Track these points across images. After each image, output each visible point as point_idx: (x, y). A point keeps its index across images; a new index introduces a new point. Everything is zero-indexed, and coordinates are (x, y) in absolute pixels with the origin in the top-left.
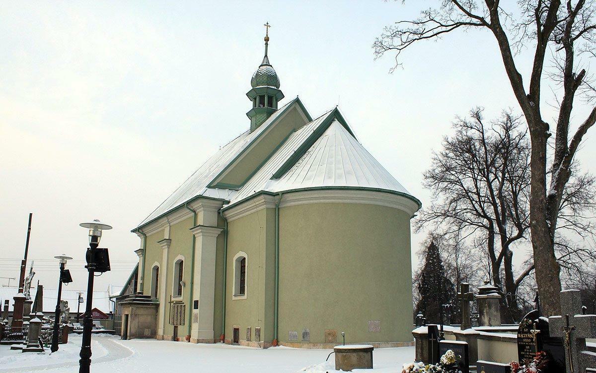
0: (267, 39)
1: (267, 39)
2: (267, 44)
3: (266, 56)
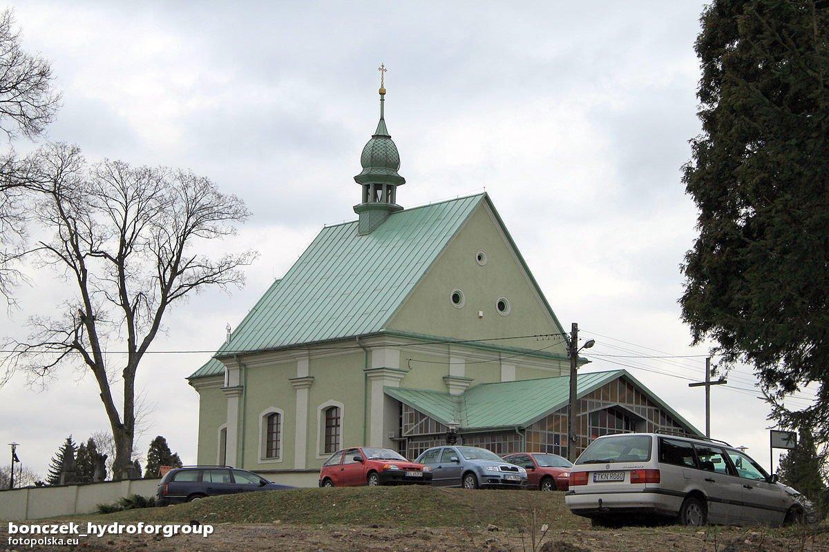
0: (382, 93)
1: (382, 93)
2: (382, 100)
3: (382, 119)
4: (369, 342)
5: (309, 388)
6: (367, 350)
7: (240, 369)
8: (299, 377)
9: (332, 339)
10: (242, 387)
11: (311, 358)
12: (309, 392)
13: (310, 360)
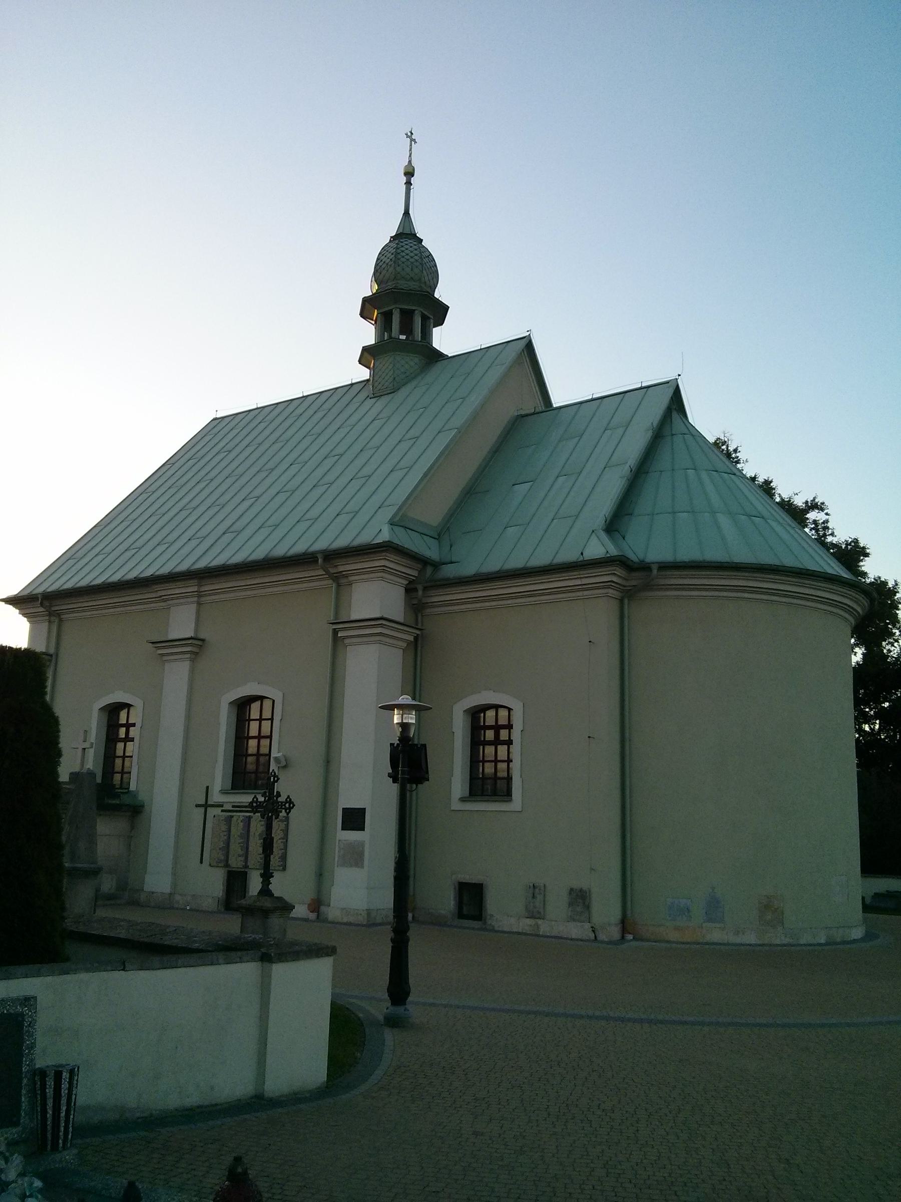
0: (409, 174)
1: (409, 174)
2: (408, 184)
3: (407, 213)
4: (344, 567)
5: (193, 660)
6: (340, 581)
7: (50, 622)
8: (171, 637)
9: (113, 583)
10: (51, 656)
11: (203, 599)
12: (192, 671)
13: (199, 604)
